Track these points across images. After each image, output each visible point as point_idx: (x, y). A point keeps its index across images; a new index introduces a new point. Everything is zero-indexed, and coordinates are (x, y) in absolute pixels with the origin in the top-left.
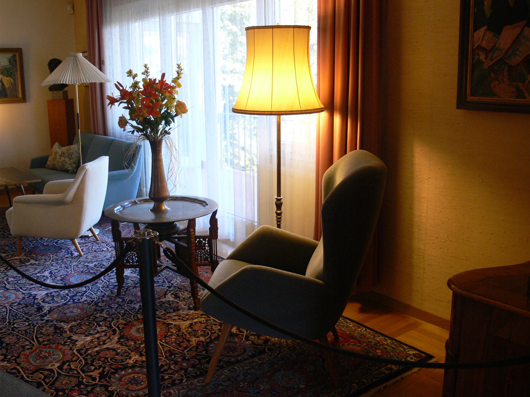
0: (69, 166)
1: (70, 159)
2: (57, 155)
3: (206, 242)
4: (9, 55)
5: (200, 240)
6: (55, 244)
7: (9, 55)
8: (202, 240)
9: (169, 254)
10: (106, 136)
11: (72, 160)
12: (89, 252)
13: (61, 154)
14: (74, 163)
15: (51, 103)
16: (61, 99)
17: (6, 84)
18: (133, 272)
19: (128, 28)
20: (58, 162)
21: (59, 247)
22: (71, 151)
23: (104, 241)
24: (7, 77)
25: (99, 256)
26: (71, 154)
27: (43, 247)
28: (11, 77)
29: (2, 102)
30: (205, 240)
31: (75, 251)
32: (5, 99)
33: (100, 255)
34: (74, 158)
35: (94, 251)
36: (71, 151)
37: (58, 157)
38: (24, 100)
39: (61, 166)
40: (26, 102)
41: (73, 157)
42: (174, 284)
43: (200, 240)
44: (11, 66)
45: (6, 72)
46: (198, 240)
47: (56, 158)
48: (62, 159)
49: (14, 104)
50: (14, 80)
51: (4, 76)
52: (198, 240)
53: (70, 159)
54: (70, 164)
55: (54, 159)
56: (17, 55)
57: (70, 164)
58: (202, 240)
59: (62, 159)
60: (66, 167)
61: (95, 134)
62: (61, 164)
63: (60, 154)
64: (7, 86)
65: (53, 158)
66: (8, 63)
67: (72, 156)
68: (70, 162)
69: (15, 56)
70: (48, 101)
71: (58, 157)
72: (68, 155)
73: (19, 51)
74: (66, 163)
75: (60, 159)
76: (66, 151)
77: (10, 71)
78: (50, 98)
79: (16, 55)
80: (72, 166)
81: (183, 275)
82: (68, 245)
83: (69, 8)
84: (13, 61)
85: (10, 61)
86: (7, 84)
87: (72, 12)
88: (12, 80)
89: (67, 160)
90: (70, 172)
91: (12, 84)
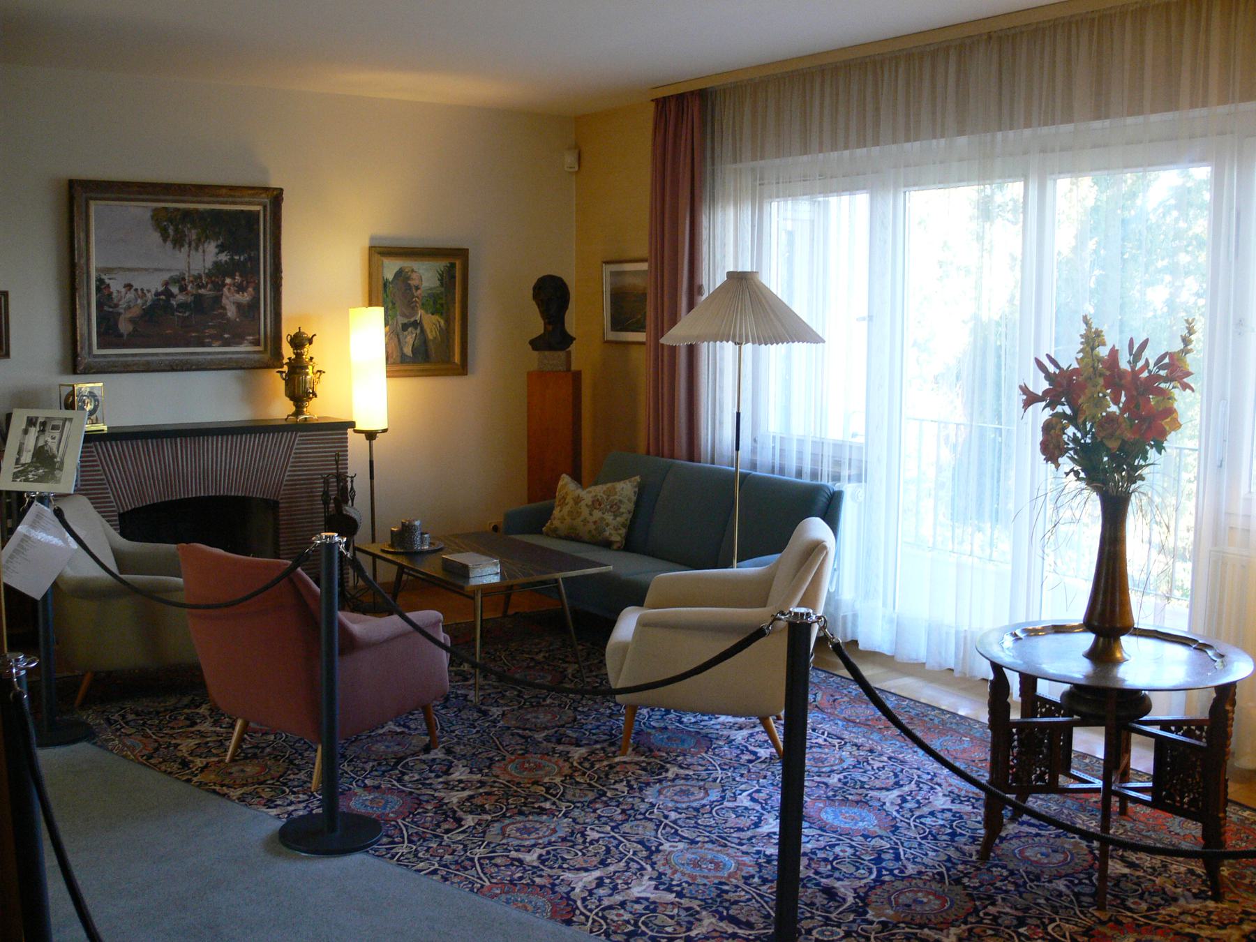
0: (613, 532)
1: (615, 516)
2: (583, 504)
3: (1204, 734)
4: (441, 264)
5: (1189, 728)
6: (395, 783)
7: (441, 264)
8: (1193, 727)
9: (1049, 776)
10: (693, 461)
11: (618, 519)
12: (504, 816)
13: (593, 502)
14: (624, 525)
15: (537, 379)
16: (560, 371)
17: (428, 331)
18: (662, 887)
19: (1055, 184)
20: (585, 521)
21: (411, 793)
22: (616, 497)
23: (486, 797)
24: (433, 314)
25: (537, 829)
26: (616, 504)
27: (366, 793)
28: (442, 314)
29: (396, 374)
30: (1201, 729)
31: (462, 810)
32: (427, 366)
33: (538, 825)
34: (623, 513)
35: (516, 811)
36: (616, 497)
37: (585, 512)
38: (463, 369)
39: (594, 532)
40: (467, 374)
41: (621, 510)
42: (842, 934)
43: (1189, 728)
44: (443, 289)
45: (431, 303)
46: (1185, 728)
47: (579, 514)
48: (597, 514)
49: (439, 378)
50: (448, 321)
51: (427, 312)
52: (1185, 728)
53: (615, 516)
54: (616, 529)
55: (574, 514)
56: (458, 263)
57: (616, 529)
58: (1193, 727)
59: (597, 514)
60: (607, 533)
61: (672, 456)
62: (593, 527)
63: (590, 503)
64: (430, 337)
65: (570, 513)
66: (438, 283)
67: (619, 508)
68: (615, 523)
69: (453, 266)
70: (530, 374)
71: (585, 512)
72: (611, 507)
73: (462, 254)
74: (608, 525)
75: (591, 514)
76: (605, 497)
77: (440, 301)
78: (534, 366)
79: (455, 264)
80: (621, 532)
81: (1194, 820)
82: (435, 790)
83: (570, 159)
84: (447, 278)
85: (441, 280)
86: (431, 331)
87: (577, 169)
88: (442, 322)
89: (609, 517)
90: (615, 547)
91: (441, 330)
